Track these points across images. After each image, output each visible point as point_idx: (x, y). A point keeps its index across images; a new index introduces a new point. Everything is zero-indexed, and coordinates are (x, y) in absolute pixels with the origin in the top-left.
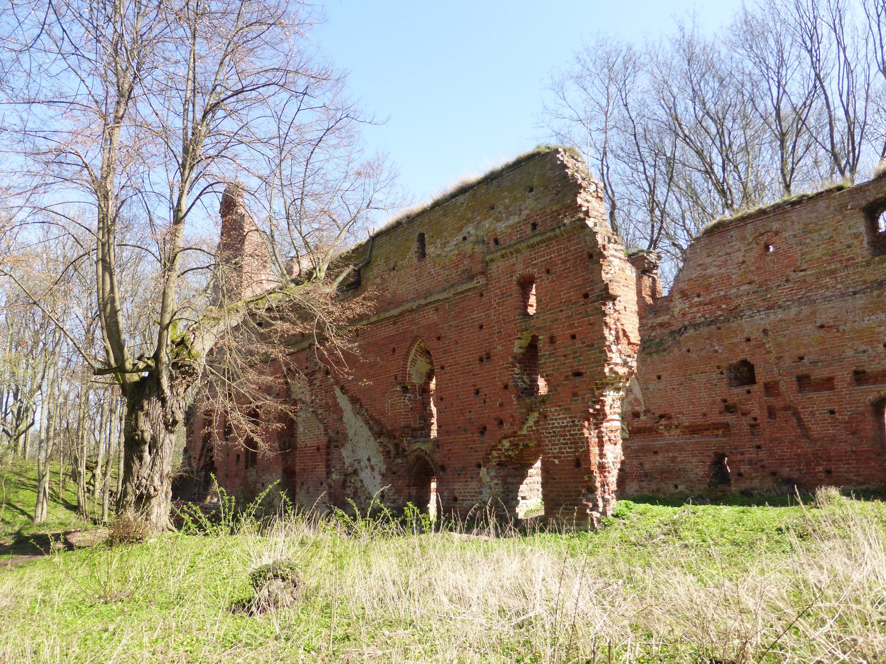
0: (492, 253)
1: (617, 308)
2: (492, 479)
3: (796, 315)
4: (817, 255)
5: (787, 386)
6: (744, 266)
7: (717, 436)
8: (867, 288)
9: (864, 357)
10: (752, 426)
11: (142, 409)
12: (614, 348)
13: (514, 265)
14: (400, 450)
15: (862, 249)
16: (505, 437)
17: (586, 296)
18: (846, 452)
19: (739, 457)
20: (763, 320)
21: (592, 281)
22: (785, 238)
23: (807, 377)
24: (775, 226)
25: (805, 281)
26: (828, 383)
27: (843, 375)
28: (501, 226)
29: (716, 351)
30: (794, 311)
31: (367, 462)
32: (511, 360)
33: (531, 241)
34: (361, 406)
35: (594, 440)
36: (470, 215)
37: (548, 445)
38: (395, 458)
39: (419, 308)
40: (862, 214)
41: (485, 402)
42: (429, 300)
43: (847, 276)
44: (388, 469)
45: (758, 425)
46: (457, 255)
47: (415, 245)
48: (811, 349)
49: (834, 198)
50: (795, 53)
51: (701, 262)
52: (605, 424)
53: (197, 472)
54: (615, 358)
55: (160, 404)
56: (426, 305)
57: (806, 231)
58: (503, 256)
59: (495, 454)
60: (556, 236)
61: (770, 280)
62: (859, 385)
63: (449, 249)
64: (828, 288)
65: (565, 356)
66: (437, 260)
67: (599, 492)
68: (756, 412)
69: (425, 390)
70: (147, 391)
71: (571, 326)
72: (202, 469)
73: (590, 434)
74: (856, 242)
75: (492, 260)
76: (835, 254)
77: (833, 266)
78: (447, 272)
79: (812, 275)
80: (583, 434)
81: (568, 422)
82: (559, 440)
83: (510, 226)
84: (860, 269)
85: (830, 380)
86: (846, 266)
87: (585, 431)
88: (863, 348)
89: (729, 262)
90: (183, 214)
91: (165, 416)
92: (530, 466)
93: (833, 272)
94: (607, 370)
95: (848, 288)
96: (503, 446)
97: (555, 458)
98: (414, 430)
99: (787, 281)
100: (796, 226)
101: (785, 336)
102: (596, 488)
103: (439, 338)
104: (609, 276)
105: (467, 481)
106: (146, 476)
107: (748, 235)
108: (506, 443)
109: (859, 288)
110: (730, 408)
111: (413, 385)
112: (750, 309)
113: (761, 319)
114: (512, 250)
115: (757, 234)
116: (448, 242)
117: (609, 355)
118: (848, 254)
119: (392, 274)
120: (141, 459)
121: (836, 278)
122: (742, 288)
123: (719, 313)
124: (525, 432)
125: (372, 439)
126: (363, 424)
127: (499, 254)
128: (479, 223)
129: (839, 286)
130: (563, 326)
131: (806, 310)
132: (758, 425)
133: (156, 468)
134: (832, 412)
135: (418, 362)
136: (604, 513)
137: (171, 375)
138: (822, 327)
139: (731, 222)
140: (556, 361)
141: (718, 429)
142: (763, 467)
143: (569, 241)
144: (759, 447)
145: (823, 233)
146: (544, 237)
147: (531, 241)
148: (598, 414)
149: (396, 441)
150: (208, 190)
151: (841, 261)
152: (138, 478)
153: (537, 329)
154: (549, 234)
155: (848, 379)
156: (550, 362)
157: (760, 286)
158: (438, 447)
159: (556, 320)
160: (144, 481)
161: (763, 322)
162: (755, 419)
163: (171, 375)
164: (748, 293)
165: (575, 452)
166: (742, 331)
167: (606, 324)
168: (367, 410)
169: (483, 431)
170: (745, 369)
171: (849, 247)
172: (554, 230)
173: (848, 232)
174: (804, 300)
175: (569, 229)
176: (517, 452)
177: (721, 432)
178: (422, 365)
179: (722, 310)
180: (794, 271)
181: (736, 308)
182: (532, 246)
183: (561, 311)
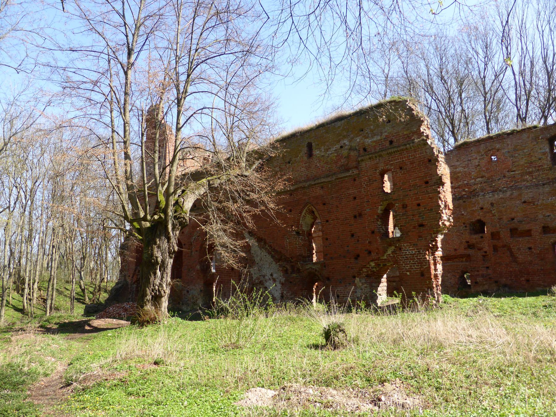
0: (362, 156)
1: (444, 189)
2: (363, 284)
3: (510, 196)
4: (521, 163)
5: (505, 235)
6: (479, 167)
7: (462, 261)
8: (550, 182)
9: (549, 219)
10: (484, 256)
11: (155, 244)
12: (444, 211)
13: (377, 163)
14: (296, 269)
15: (547, 161)
16: (372, 261)
17: (427, 183)
18: (538, 270)
19: (476, 273)
20: (490, 197)
21: (431, 174)
22: (503, 153)
23: (516, 229)
24: (498, 146)
25: (514, 177)
26: (528, 233)
27: (536, 228)
28: (368, 141)
29: (463, 215)
30: (508, 193)
31: (270, 277)
32: (376, 217)
33: (390, 151)
34: (265, 243)
35: (432, 262)
36: (345, 134)
37: (402, 265)
38: (291, 273)
39: (310, 186)
40: (547, 142)
41: (358, 241)
42: (317, 182)
43: (539, 175)
44: (285, 281)
45: (488, 255)
46: (336, 156)
47: (305, 150)
48: (518, 214)
49: (532, 132)
50: (496, 45)
51: (453, 164)
52: (437, 253)
53: (131, 285)
54: (445, 217)
55: (166, 241)
56: (315, 184)
57: (515, 150)
58: (370, 158)
59: (365, 270)
60: (407, 149)
61: (495, 176)
62: (544, 234)
63: (330, 152)
64: (528, 181)
65: (413, 215)
66: (322, 159)
67: (435, 290)
68: (486, 248)
69: (310, 234)
70: (158, 233)
71: (417, 199)
72: (134, 283)
73: (430, 258)
74: (543, 157)
75: (362, 160)
76: (531, 163)
77: (531, 170)
78: (329, 166)
79: (519, 174)
80: (426, 258)
81: (416, 252)
82: (410, 262)
83: (375, 142)
84: (546, 172)
85: (529, 231)
86: (538, 170)
87: (427, 256)
88: (548, 214)
89: (470, 165)
90: (181, 126)
91: (169, 248)
92: (382, 277)
93: (530, 173)
94: (440, 223)
95: (539, 181)
96: (370, 265)
97: (407, 271)
98: (304, 257)
99: (504, 177)
100: (510, 147)
101: (503, 207)
102: (434, 288)
103: (324, 204)
104: (440, 172)
105: (346, 286)
106: (158, 284)
107: (481, 151)
108: (373, 264)
109: (545, 182)
110: (470, 246)
111: (303, 231)
112: (482, 192)
113: (490, 197)
114: (376, 155)
115: (487, 150)
116: (330, 148)
117: (442, 215)
118: (539, 163)
119: (288, 165)
120: (155, 274)
121: (532, 176)
122: (478, 180)
123: (464, 193)
124: (386, 258)
125: (274, 263)
126: (267, 254)
127: (368, 157)
128: (353, 138)
129: (534, 180)
130: (412, 199)
131: (516, 193)
132: (488, 255)
133: (164, 279)
134: (530, 248)
135: (307, 217)
136: (438, 301)
137: (173, 223)
138: (525, 202)
139: (471, 142)
140: (407, 218)
141: (463, 258)
142: (490, 278)
143: (415, 152)
144: (488, 268)
145: (525, 151)
146: (399, 149)
147: (390, 151)
148: (433, 247)
149: (292, 264)
150: (198, 112)
151: (535, 167)
152: (153, 285)
153: (394, 200)
154: (402, 147)
155: (540, 231)
156: (403, 219)
157: (488, 179)
158: (325, 267)
159: (407, 195)
160: (157, 287)
161: (491, 199)
162: (486, 252)
163: (173, 223)
164: (481, 183)
165: (421, 268)
166: (479, 204)
167: (440, 198)
168: (270, 246)
169: (357, 257)
170: (478, 225)
171: (540, 159)
172: (405, 145)
173: (539, 151)
174: (514, 187)
175: (416, 145)
176: (378, 269)
177: (464, 259)
178: (309, 219)
179: (466, 191)
180: (508, 171)
181: (474, 190)
182: (390, 154)
183: (410, 190)
